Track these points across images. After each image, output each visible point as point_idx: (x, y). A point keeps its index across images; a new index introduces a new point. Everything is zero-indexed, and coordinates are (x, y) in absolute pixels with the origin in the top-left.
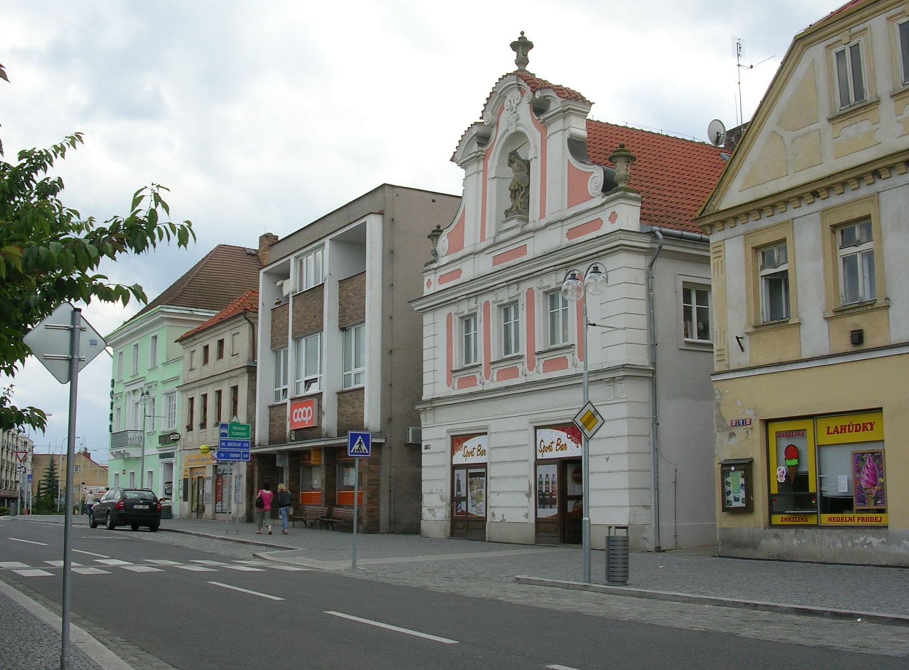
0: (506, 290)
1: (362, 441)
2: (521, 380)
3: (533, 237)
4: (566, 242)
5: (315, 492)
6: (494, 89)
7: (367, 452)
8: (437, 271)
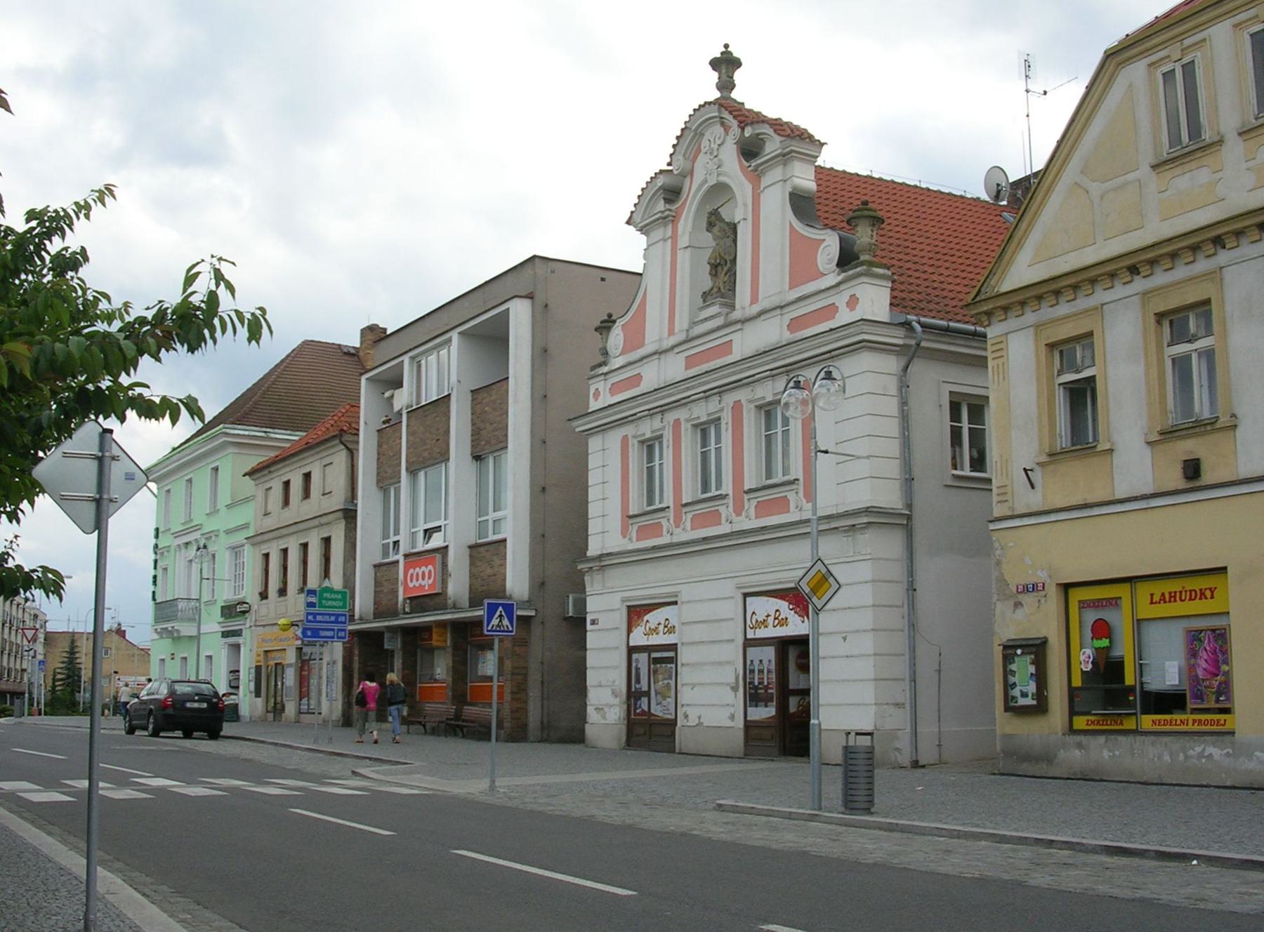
0: (704, 403)
1: (503, 613)
2: (724, 528)
3: (741, 329)
4: (788, 336)
5: (438, 685)
6: (687, 124)
7: (511, 629)
8: (608, 377)
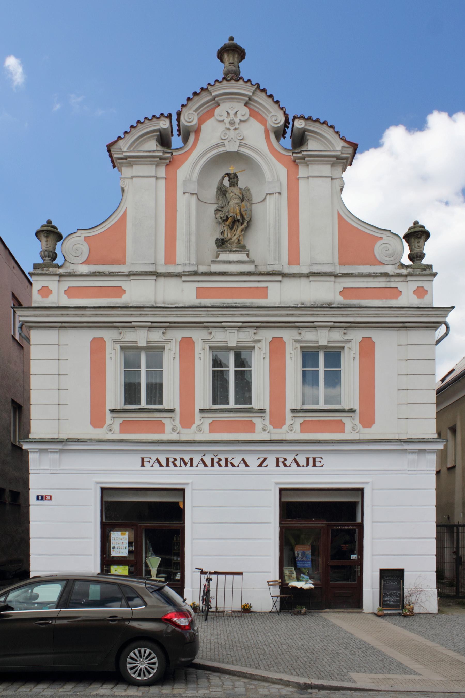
0: (236, 332)
2: (168, 435)
3: (280, 281)
4: (339, 299)
6: (209, 87)
8: (63, 279)
